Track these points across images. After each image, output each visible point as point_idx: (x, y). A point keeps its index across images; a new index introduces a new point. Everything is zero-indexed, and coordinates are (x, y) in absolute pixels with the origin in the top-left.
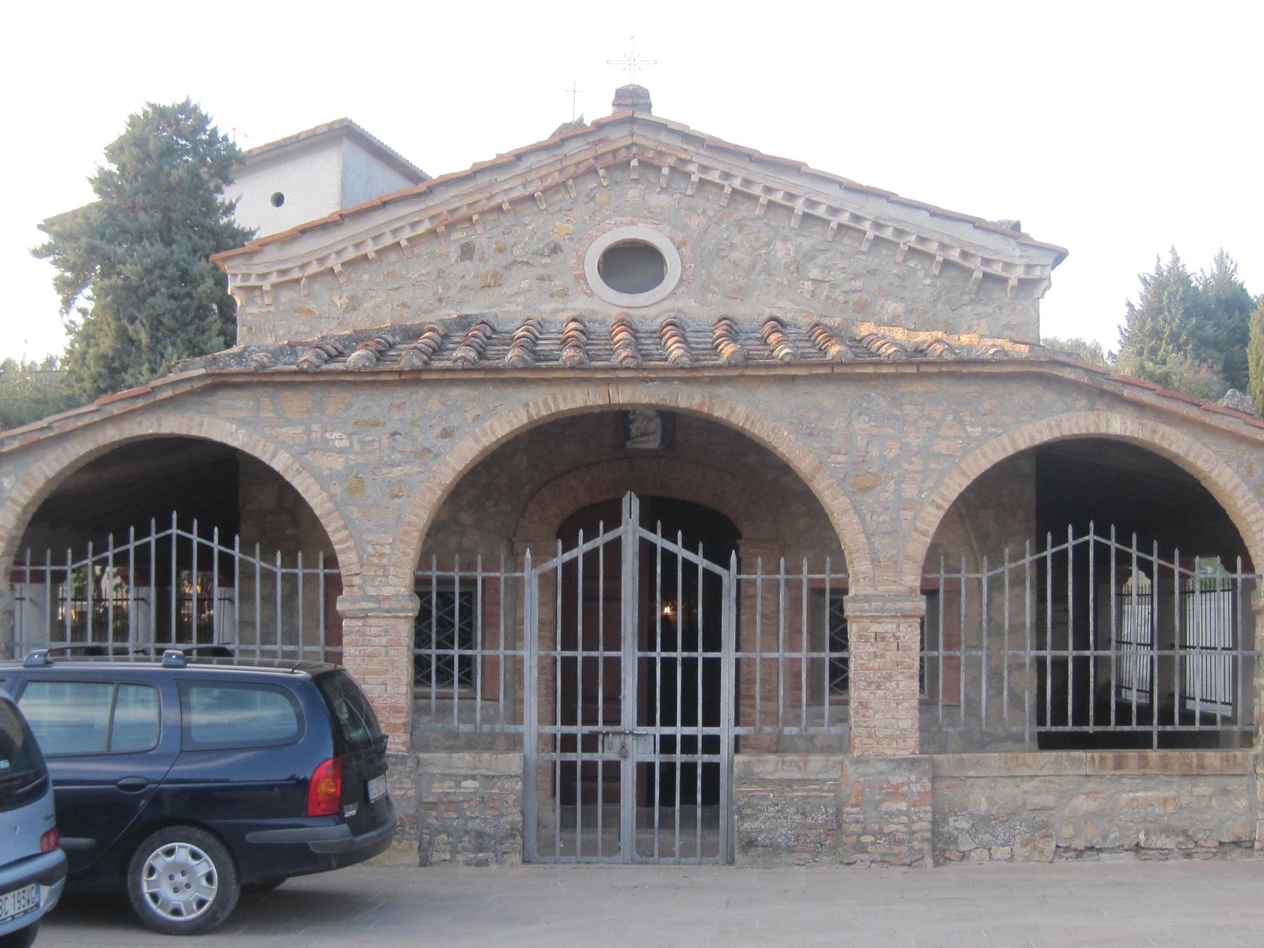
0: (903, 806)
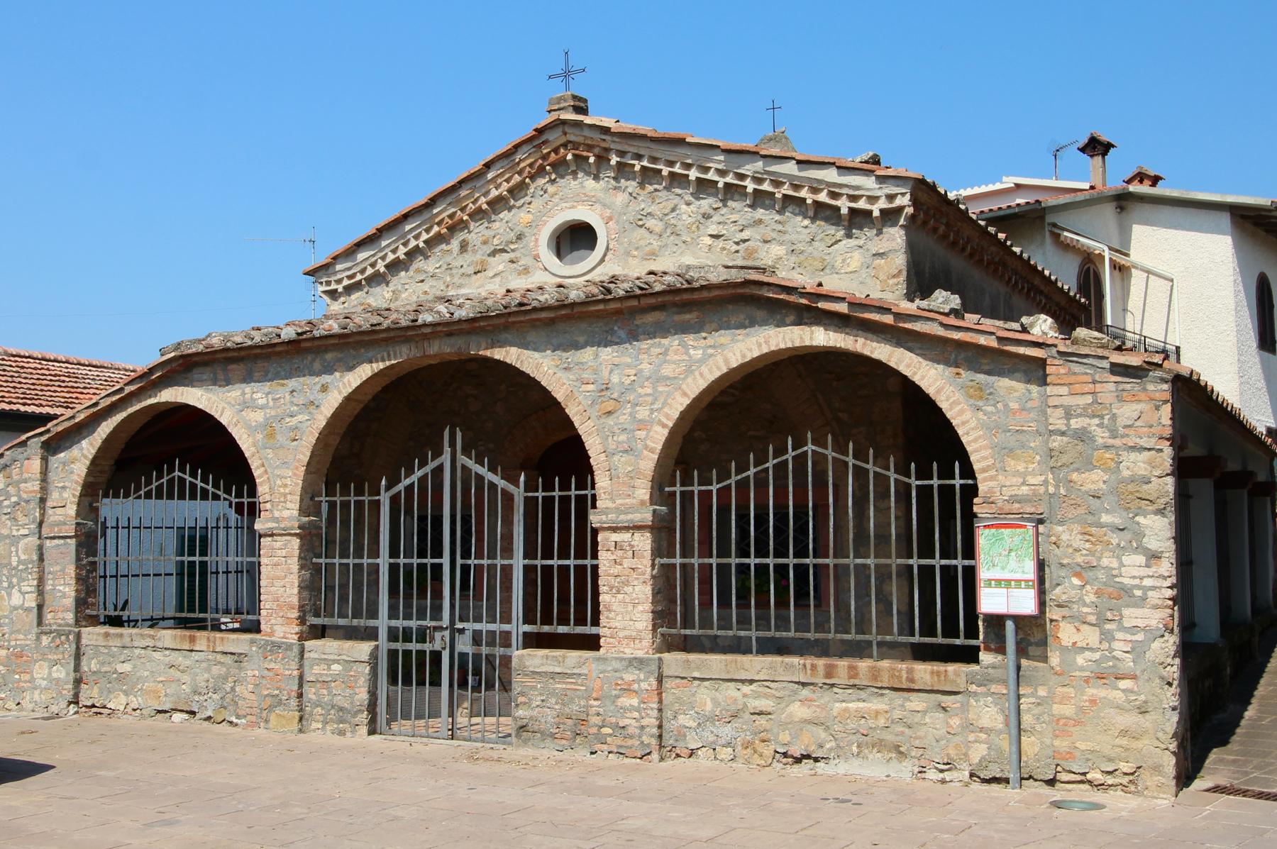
0: (635, 702)
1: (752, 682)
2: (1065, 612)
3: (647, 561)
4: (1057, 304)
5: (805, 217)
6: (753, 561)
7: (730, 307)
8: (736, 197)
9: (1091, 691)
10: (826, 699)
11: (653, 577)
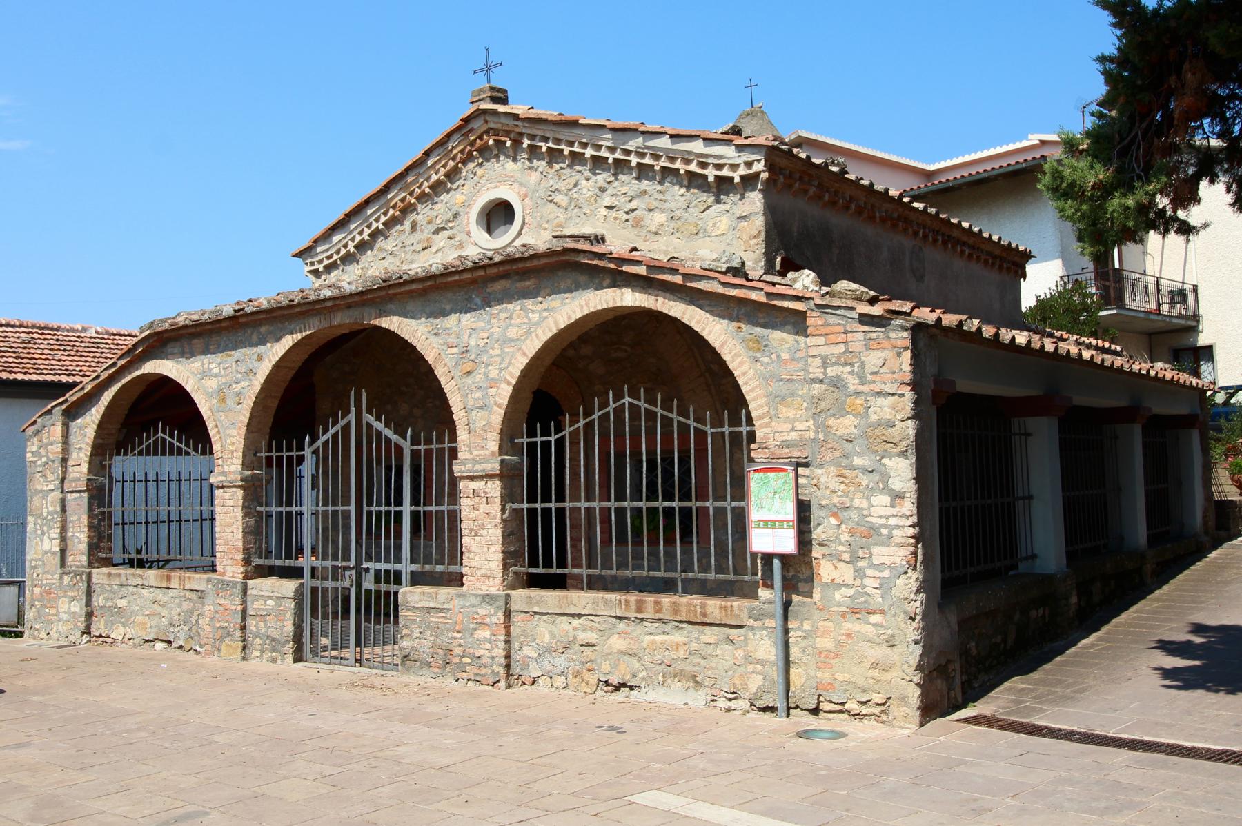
0: (487, 634)
1: (580, 616)
2: (825, 550)
4: (989, 253)
6: (613, 504)
7: (560, 273)
8: (626, 171)
11: (503, 521)
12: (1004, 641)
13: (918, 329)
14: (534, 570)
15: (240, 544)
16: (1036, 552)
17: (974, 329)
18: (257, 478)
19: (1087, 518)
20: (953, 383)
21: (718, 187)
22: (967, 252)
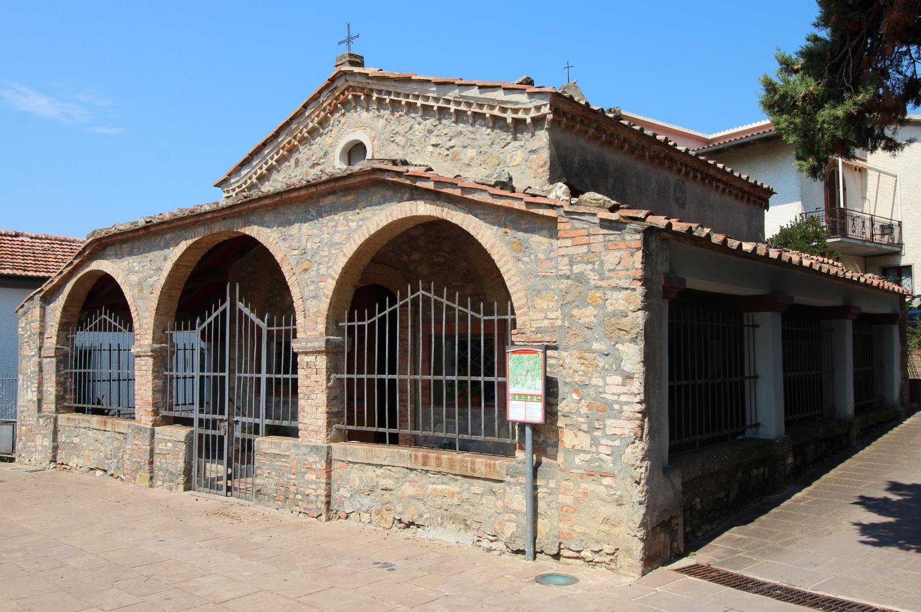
0: (314, 477)
1: (381, 466)
3: (324, 376)
5: (488, 128)
7: (372, 190)
8: (447, 116)
9: (584, 485)
10: (424, 481)
11: (328, 388)
12: (727, 496)
13: (650, 233)
14: (351, 427)
15: (150, 399)
16: (759, 421)
17: (703, 235)
18: (340, 345)
19: (804, 393)
20: (684, 281)
21: (515, 127)
22: (721, 187)
